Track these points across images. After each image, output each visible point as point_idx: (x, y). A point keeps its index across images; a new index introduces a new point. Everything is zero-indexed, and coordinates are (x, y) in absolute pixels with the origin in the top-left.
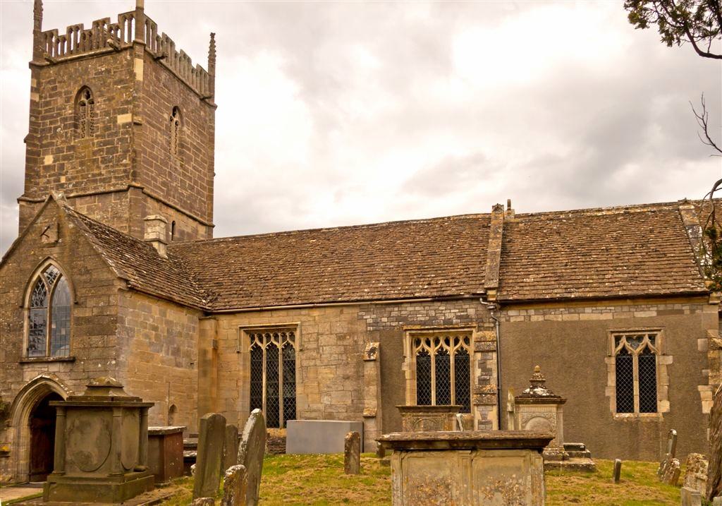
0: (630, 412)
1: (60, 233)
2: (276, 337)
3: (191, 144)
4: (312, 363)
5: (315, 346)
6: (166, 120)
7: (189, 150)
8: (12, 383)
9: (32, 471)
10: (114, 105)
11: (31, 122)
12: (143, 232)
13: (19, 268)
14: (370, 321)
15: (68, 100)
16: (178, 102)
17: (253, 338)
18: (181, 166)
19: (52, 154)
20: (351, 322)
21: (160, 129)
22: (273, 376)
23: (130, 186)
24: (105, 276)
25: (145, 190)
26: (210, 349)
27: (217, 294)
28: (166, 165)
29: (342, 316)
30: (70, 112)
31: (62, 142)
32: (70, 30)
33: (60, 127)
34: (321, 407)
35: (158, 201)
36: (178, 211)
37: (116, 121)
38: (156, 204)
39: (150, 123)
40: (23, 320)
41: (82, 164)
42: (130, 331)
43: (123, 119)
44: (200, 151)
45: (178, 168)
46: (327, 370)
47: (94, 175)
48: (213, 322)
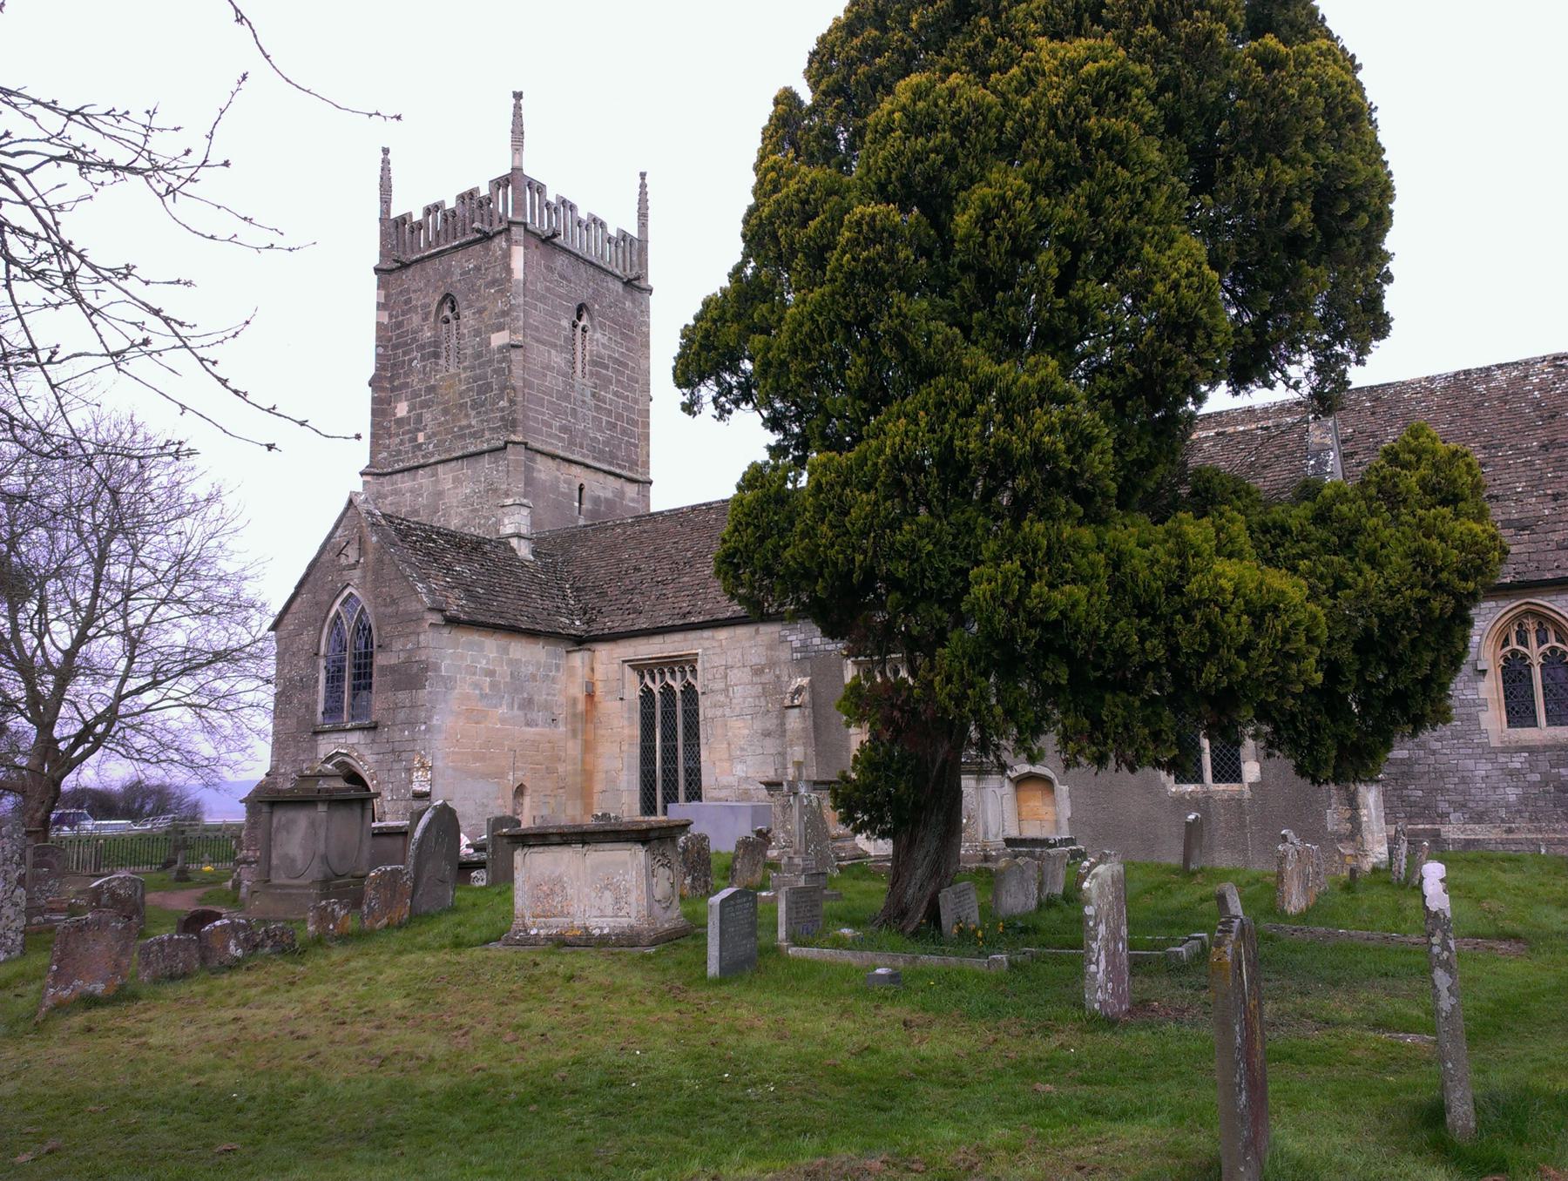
0: (1196, 781)
1: (362, 551)
2: (673, 673)
4: (719, 712)
5: (722, 686)
7: (606, 367)
11: (378, 355)
12: (499, 522)
14: (797, 644)
15: (425, 319)
16: (585, 296)
17: (642, 677)
18: (593, 395)
20: (770, 647)
21: (554, 346)
22: (669, 735)
23: (507, 443)
24: (414, 606)
25: (532, 444)
26: (580, 695)
28: (567, 398)
29: (759, 638)
31: (421, 380)
32: (428, 211)
34: (732, 780)
35: (554, 457)
36: (588, 466)
38: (550, 462)
39: (538, 341)
41: (446, 412)
42: (449, 683)
43: (499, 339)
46: (740, 724)
47: (461, 428)
48: (587, 654)
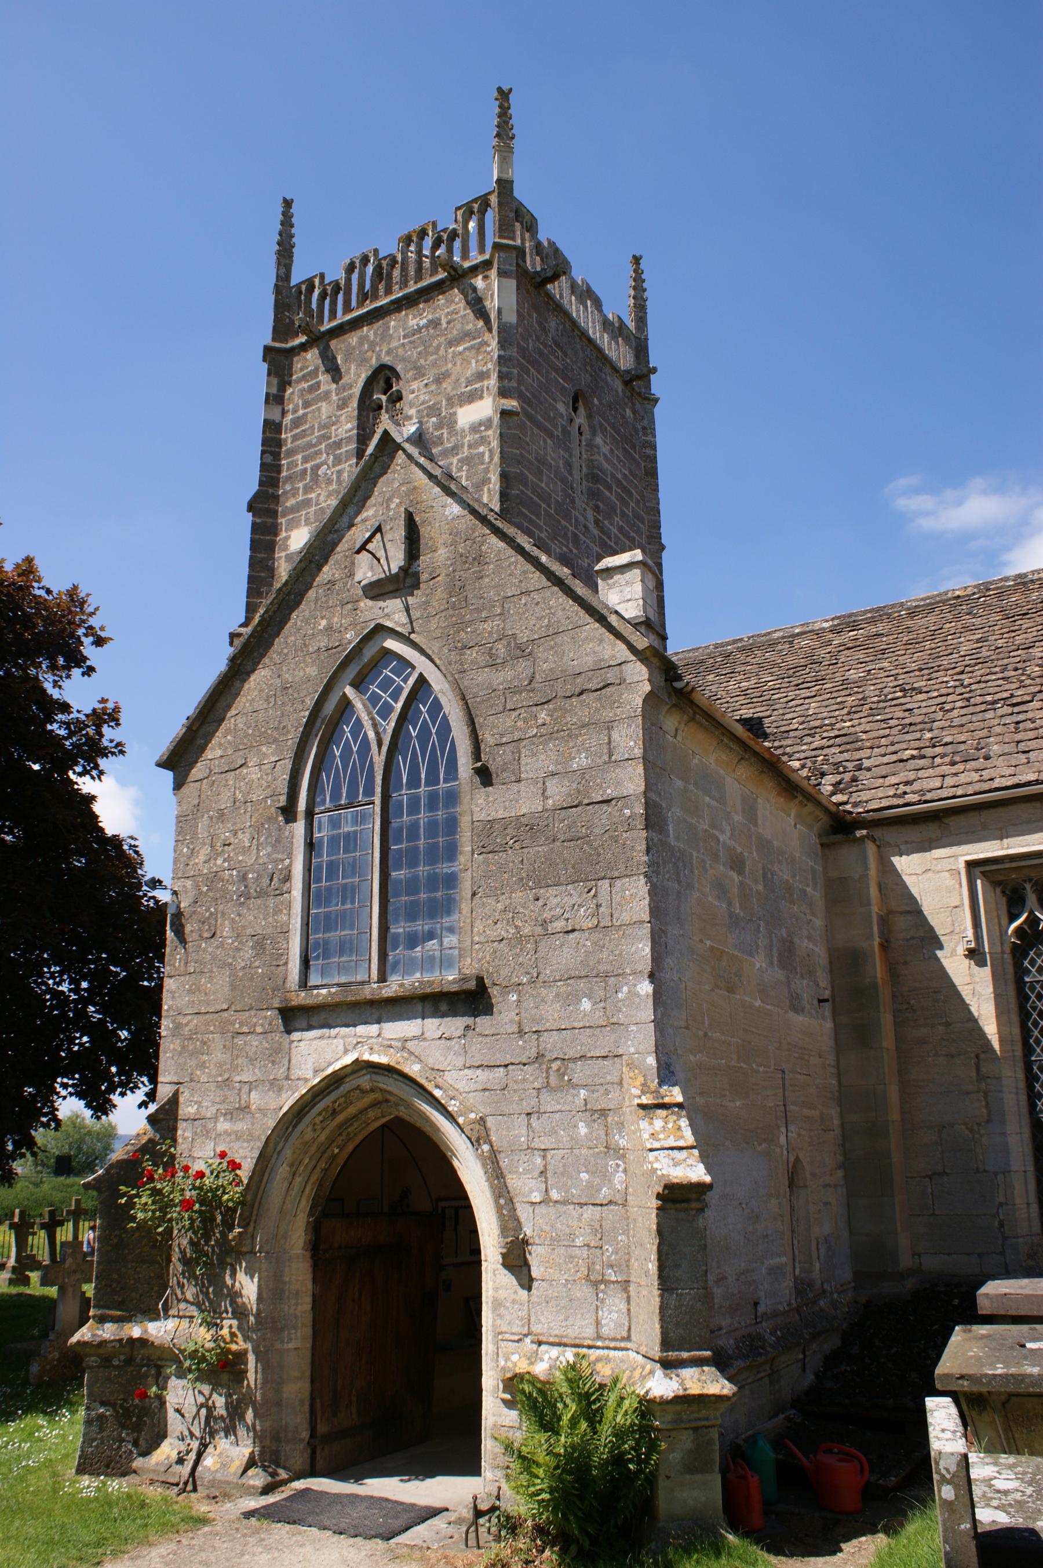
3: (613, 476)
6: (562, 417)
7: (610, 489)
8: (251, 1085)
9: (322, 1429)
10: (449, 389)
11: (262, 465)
13: (278, 682)
18: (597, 522)
19: (306, 525)
21: (551, 435)
27: (850, 766)
30: (349, 426)
32: (351, 268)
33: (326, 463)
37: (456, 422)
40: (290, 856)
44: (630, 494)
45: (591, 526)
